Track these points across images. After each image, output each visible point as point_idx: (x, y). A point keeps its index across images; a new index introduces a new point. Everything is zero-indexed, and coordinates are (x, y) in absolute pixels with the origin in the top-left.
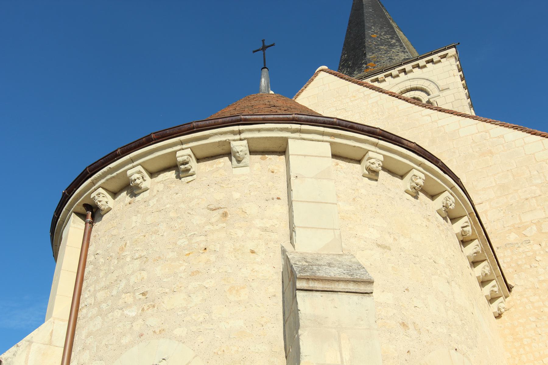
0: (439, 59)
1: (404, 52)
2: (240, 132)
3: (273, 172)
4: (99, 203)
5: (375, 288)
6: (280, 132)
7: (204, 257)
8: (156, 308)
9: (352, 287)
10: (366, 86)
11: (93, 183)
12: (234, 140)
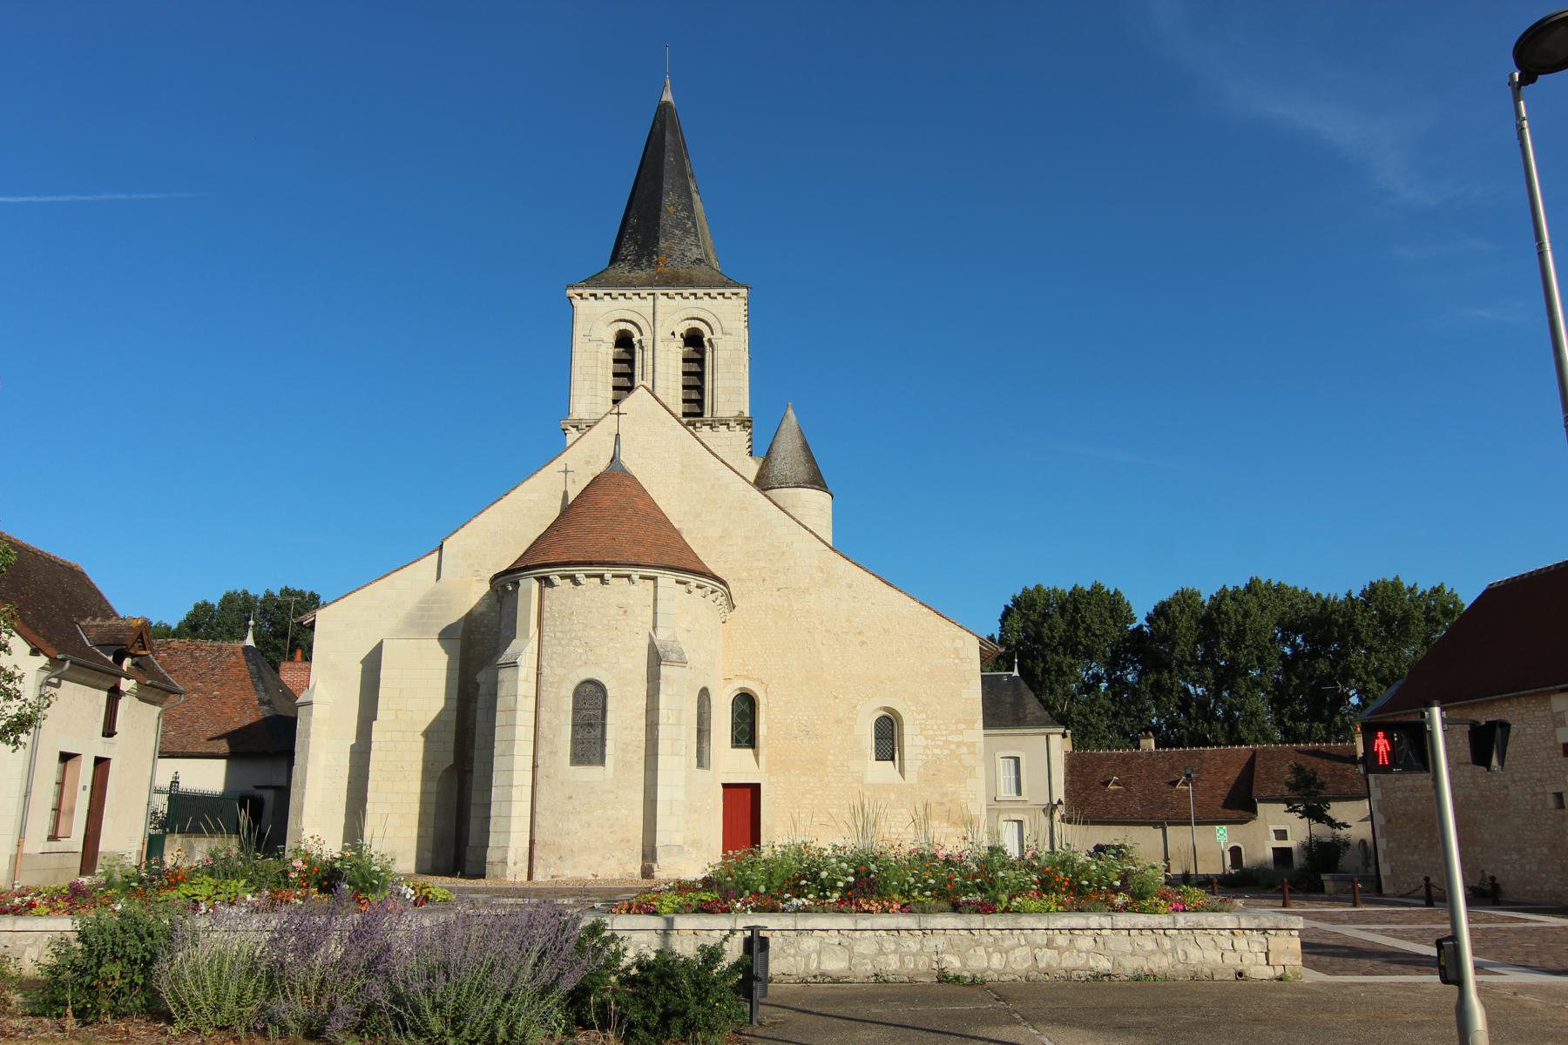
1: (698, 247)
9: (680, 664)
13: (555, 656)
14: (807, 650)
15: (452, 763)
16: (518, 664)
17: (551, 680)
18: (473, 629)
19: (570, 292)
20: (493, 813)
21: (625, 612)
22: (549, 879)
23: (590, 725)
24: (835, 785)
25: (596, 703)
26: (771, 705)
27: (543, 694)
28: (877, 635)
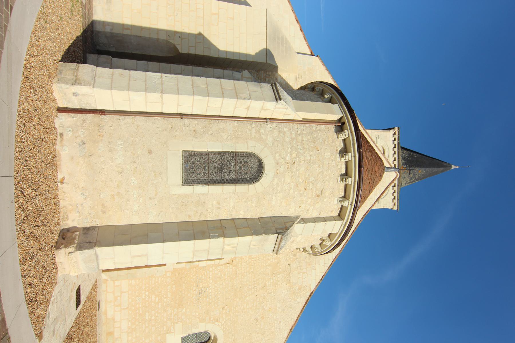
0: (394, 202)
2: (351, 205)
3: (332, 212)
4: (342, 134)
5: (274, 254)
6: (347, 219)
7: (303, 189)
8: (287, 169)
9: (276, 249)
10: (381, 194)
11: (351, 132)
12: (349, 202)
13: (282, 135)
14: (253, 287)
15: (180, 52)
16: (279, 102)
17: (262, 131)
18: (268, 73)
19: (396, 129)
20: (133, 72)
21: (318, 196)
22: (59, 131)
23: (221, 169)
24: (165, 315)
25: (241, 173)
26: (219, 268)
27: (248, 124)
28: (261, 327)
